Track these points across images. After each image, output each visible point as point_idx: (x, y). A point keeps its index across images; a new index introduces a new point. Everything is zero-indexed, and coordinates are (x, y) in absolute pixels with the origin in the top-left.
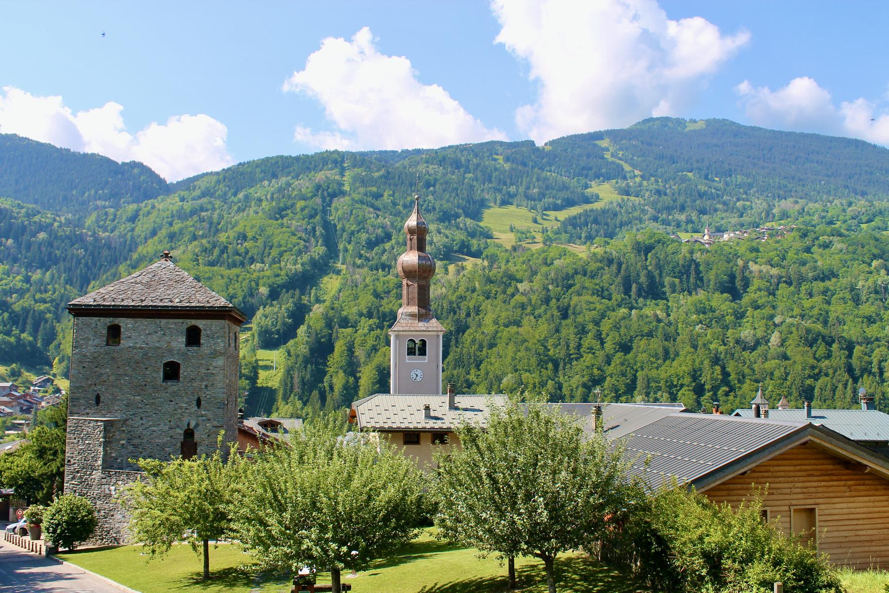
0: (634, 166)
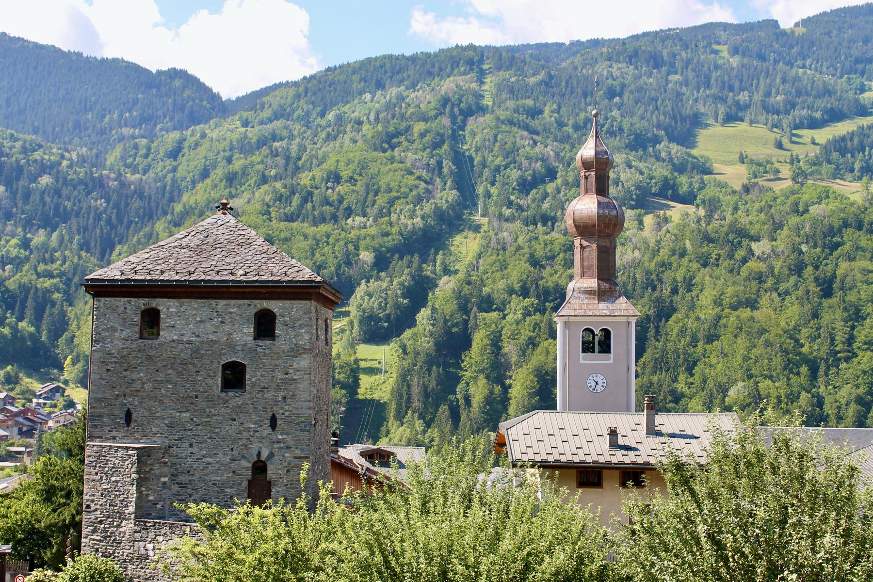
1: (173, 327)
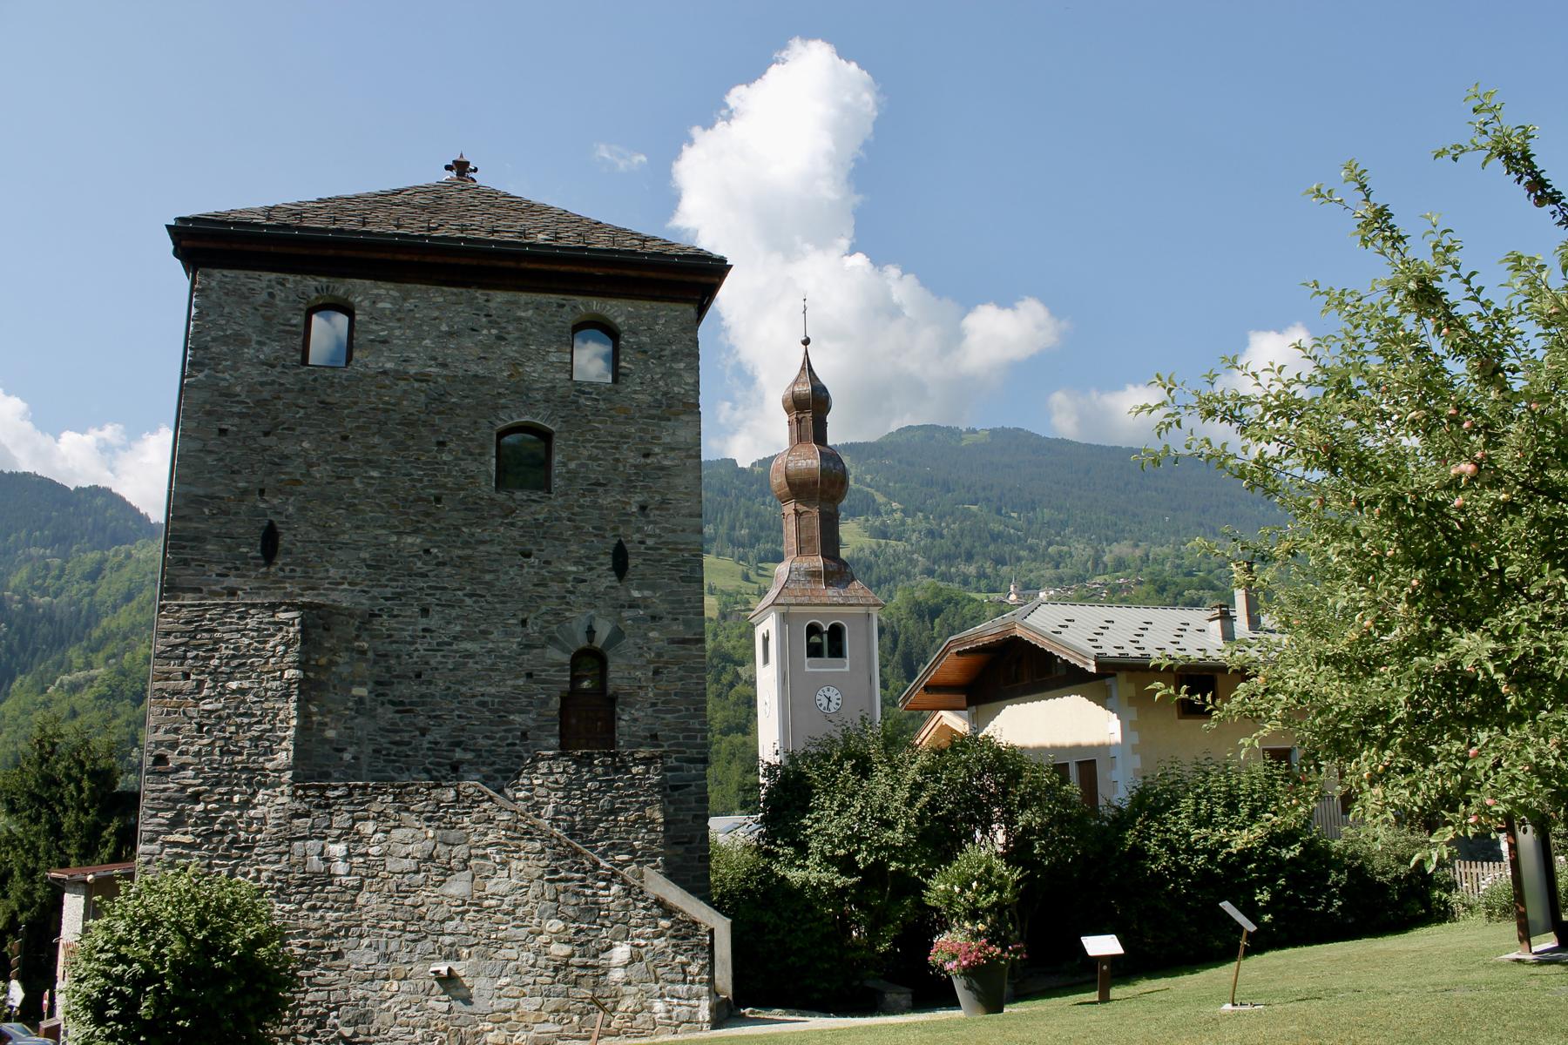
0: (891, 496)
1: (384, 342)
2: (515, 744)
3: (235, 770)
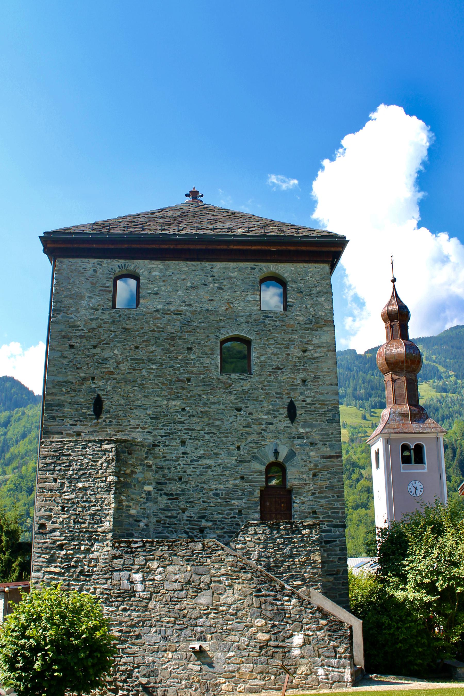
0: (447, 367)
1: (157, 294)
2: (235, 517)
3: (82, 532)
